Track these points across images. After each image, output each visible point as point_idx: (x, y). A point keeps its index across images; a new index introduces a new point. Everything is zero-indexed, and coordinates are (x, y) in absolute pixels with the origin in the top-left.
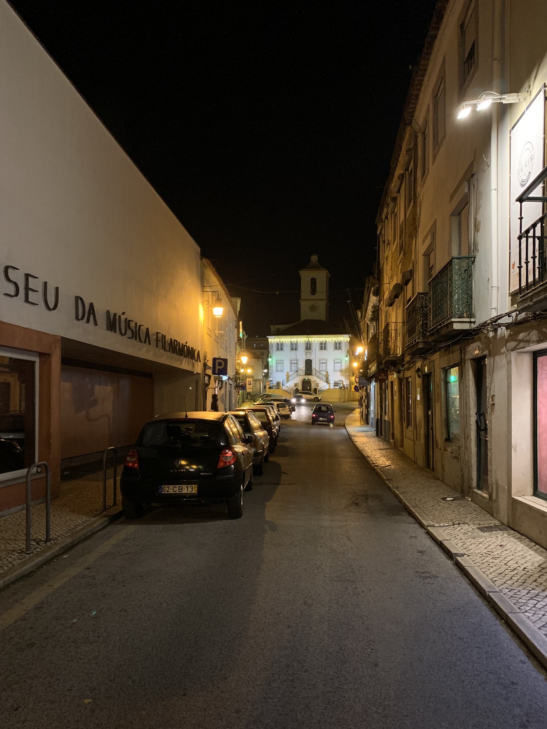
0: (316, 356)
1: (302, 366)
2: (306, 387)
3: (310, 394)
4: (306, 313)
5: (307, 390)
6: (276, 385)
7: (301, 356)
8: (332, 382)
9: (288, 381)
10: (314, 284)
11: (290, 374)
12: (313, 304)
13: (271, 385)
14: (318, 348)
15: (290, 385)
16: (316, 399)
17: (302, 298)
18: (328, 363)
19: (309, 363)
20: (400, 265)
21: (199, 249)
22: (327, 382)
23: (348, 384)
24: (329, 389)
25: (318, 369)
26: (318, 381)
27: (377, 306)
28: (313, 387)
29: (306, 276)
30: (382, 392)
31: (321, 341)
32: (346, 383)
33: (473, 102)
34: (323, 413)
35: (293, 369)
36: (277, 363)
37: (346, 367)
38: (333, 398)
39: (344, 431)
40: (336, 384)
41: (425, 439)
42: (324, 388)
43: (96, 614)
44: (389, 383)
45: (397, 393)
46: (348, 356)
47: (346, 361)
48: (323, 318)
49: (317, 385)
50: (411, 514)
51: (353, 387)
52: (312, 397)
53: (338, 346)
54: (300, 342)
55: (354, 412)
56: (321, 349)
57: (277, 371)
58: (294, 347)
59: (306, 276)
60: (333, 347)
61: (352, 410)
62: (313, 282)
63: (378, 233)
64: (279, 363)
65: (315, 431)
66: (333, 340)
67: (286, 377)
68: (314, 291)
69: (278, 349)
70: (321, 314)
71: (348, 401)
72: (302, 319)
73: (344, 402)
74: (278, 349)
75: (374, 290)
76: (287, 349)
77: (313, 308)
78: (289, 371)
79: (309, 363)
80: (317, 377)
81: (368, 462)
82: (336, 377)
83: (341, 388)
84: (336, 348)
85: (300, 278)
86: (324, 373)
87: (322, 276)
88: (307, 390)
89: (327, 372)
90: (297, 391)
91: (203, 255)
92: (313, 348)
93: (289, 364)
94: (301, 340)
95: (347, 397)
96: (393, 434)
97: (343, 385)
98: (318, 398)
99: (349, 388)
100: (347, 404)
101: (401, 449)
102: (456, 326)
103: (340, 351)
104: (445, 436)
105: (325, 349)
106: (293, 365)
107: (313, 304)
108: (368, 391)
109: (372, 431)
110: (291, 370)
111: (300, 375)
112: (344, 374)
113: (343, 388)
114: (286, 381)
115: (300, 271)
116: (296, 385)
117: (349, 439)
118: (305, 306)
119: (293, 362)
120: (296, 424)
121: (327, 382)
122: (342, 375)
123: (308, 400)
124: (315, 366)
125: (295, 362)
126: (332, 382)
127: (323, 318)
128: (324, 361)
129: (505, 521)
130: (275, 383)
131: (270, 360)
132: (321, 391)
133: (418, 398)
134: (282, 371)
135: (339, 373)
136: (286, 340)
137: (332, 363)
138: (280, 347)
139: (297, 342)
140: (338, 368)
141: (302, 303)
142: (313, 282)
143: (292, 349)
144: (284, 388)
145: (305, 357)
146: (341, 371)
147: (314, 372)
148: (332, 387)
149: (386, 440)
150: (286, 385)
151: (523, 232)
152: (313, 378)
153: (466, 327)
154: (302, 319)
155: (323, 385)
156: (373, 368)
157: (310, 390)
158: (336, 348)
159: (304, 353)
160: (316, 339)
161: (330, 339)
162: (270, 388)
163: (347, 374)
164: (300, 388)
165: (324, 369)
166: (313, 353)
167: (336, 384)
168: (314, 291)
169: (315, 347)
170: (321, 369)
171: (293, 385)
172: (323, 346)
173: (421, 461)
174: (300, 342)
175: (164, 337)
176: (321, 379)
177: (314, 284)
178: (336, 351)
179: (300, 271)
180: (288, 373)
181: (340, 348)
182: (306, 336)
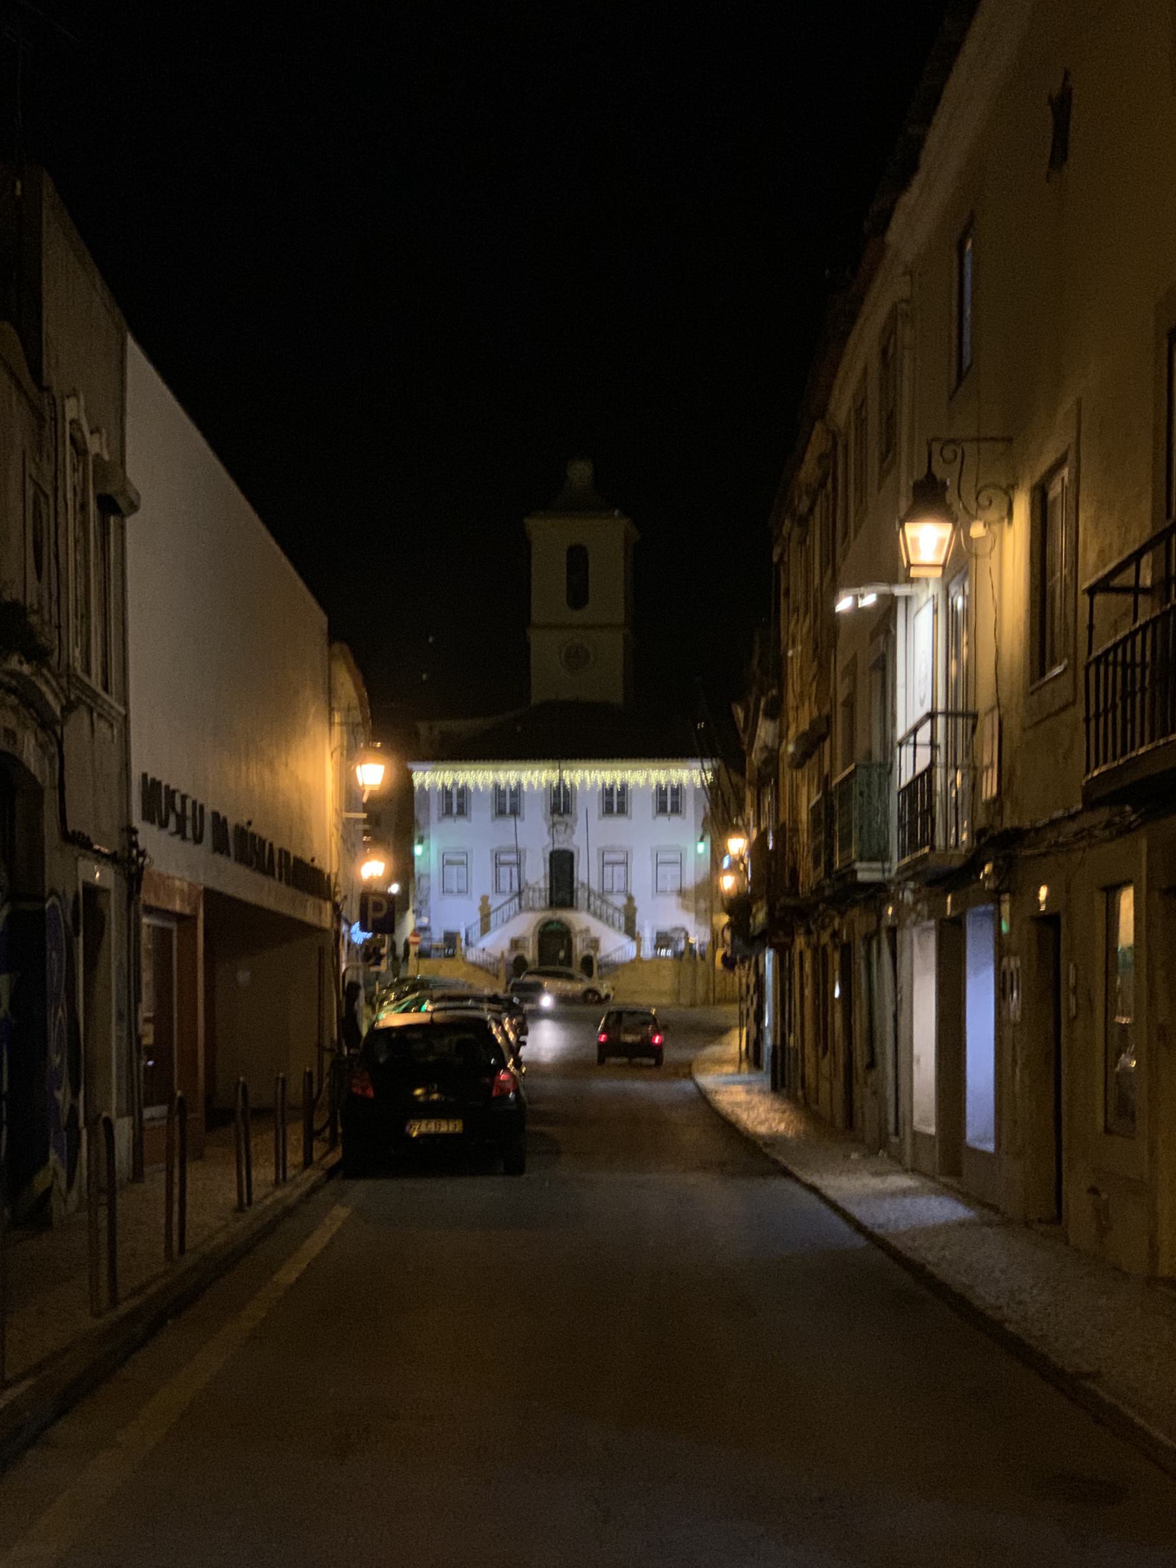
0: (590, 838)
1: (537, 873)
2: (555, 944)
3: (570, 977)
4: (550, 673)
5: (554, 959)
6: (441, 944)
7: (535, 838)
8: (648, 936)
9: (485, 929)
10: (579, 570)
11: (495, 902)
12: (577, 640)
13: (426, 944)
14: (596, 807)
15: (493, 945)
16: (591, 997)
17: (536, 616)
18: (634, 865)
19: (562, 865)
20: (814, 684)
21: (325, 619)
22: (630, 930)
23: (707, 938)
24: (638, 959)
25: (595, 886)
26: (597, 928)
27: (772, 750)
28: (580, 948)
29: (549, 537)
30: (784, 971)
31: (608, 782)
32: (698, 936)
33: (857, 591)
34: (627, 1038)
35: (505, 884)
36: (446, 863)
37: (699, 879)
38: (655, 995)
39: (688, 1086)
40: (663, 940)
41: (845, 1070)
42: (617, 957)
43: (770, 914)
44: (797, 957)
45: (810, 978)
46: (708, 839)
47: (698, 856)
48: (617, 697)
49: (595, 944)
50: (787, 1174)
51: (720, 953)
52: (578, 987)
53: (668, 801)
54: (530, 784)
55: (726, 1039)
56: (608, 810)
57: (444, 891)
58: (507, 804)
59: (549, 537)
60: (650, 806)
61: (718, 1032)
62: (577, 558)
63: (775, 559)
64: (449, 863)
65: (604, 1085)
66: (653, 781)
67: (478, 917)
68: (578, 596)
69: (448, 812)
70: (606, 679)
71: (706, 1002)
72: (536, 698)
73: (693, 1005)
74: (448, 812)
75: (766, 704)
76: (482, 812)
77: (576, 658)
78: (488, 890)
79: (562, 865)
80: (595, 914)
81: (737, 1131)
82: (664, 914)
83: (678, 956)
84: (662, 809)
85: (528, 545)
86: (620, 901)
87: (608, 539)
88: (554, 959)
89: (630, 899)
90: (519, 965)
91: (335, 635)
92: (579, 808)
93: (489, 866)
94: (534, 777)
95: (701, 987)
96: (803, 1077)
97: (690, 946)
98: (594, 992)
99: (708, 957)
100: (697, 1014)
101: (814, 1107)
102: (862, 876)
103: (675, 819)
104: (867, 1060)
105: (622, 810)
106: (504, 871)
107: (577, 640)
108: (761, 971)
109: (764, 1079)
110: (497, 890)
111: (532, 909)
112: (691, 904)
113: (688, 957)
114: (477, 929)
115: (526, 520)
116: (515, 944)
117: (703, 1098)
118: (545, 650)
119: (503, 858)
120: (536, 1068)
121: (630, 930)
122: (685, 908)
123: (563, 999)
124: (585, 873)
125: (512, 858)
126: (648, 936)
127: (617, 697)
128: (620, 857)
129: (909, 1166)
130: (437, 936)
131: (418, 850)
132: (607, 965)
133: (837, 993)
134: (464, 892)
135: (674, 901)
136: (479, 777)
137: (649, 866)
138: (456, 803)
139: (519, 785)
140: (671, 884)
141: (536, 639)
142: (577, 558)
143: (500, 812)
144: (473, 955)
145: (547, 840)
146: (681, 893)
147: (581, 895)
148: (648, 951)
149: (791, 1098)
150: (481, 945)
151: (1133, 567)
152: (580, 920)
153: (876, 877)
154: (536, 698)
155: (615, 946)
156: (760, 917)
157: (568, 960)
158: (662, 809)
159: (544, 827)
160: (589, 777)
161: (643, 776)
162: (423, 954)
163: (703, 905)
164: (530, 953)
165: (619, 884)
166: (580, 827)
167: (663, 940)
168: (578, 596)
169: (588, 808)
170: (608, 886)
171: (506, 945)
172: (615, 802)
173: (839, 1122)
174: (530, 784)
175: (287, 854)
176: (609, 922)
177: (579, 570)
178: (663, 820)
179: (526, 520)
180: (485, 899)
181: (676, 809)
182: (550, 764)
